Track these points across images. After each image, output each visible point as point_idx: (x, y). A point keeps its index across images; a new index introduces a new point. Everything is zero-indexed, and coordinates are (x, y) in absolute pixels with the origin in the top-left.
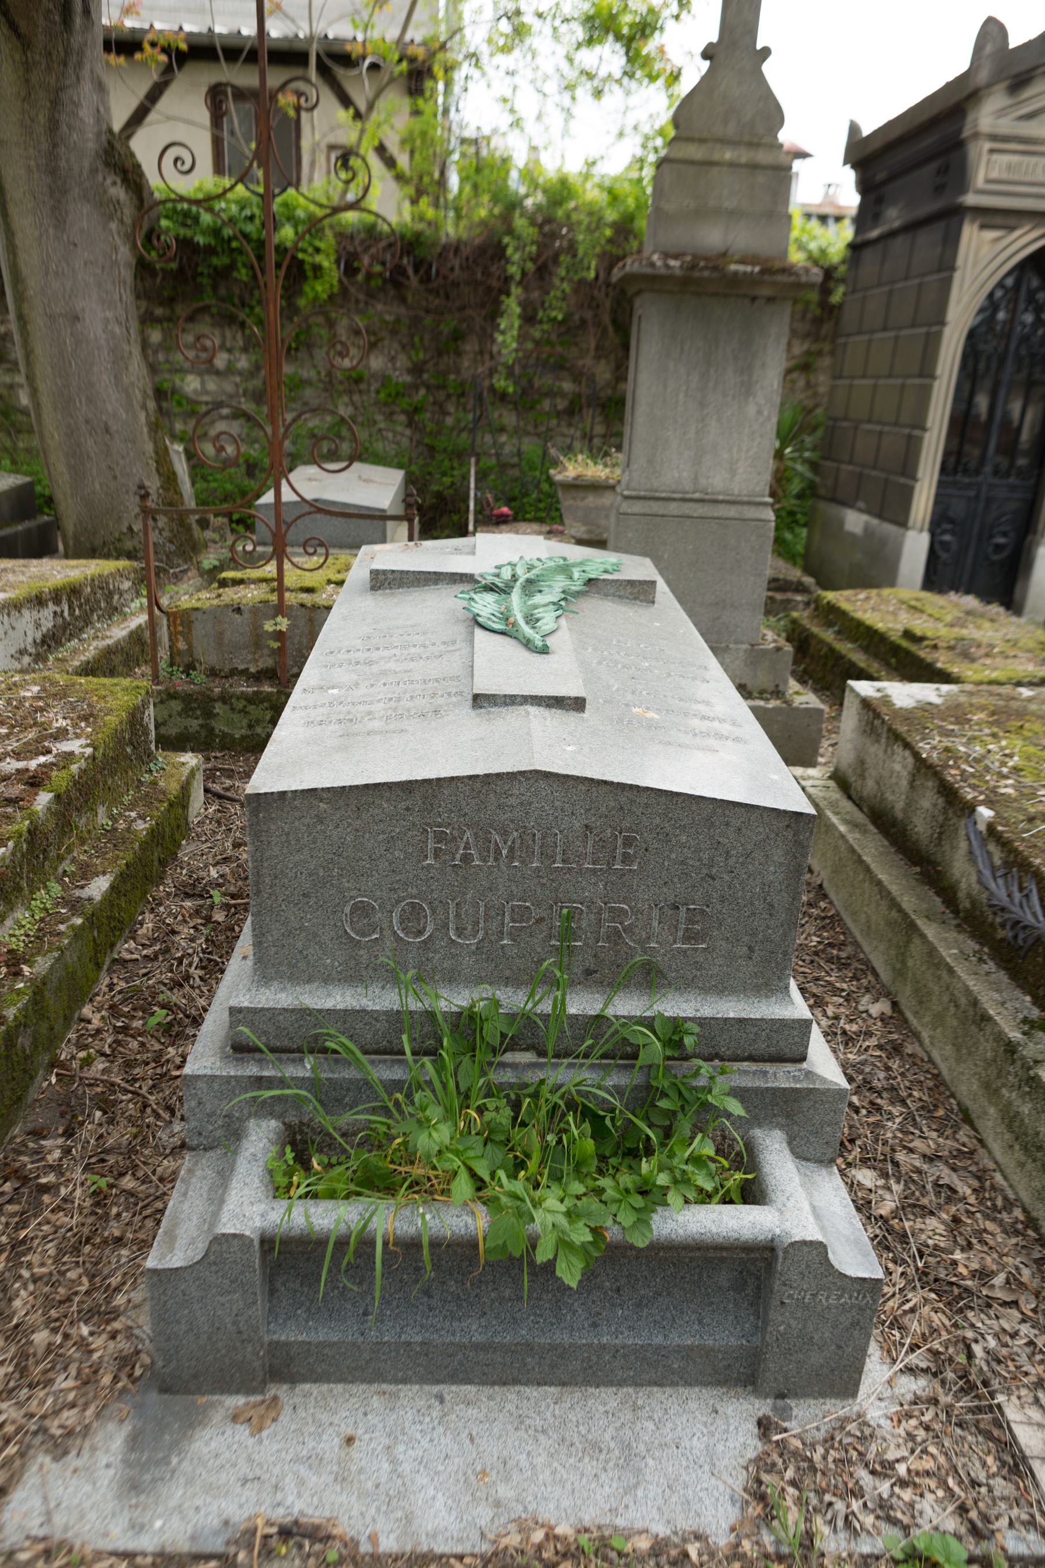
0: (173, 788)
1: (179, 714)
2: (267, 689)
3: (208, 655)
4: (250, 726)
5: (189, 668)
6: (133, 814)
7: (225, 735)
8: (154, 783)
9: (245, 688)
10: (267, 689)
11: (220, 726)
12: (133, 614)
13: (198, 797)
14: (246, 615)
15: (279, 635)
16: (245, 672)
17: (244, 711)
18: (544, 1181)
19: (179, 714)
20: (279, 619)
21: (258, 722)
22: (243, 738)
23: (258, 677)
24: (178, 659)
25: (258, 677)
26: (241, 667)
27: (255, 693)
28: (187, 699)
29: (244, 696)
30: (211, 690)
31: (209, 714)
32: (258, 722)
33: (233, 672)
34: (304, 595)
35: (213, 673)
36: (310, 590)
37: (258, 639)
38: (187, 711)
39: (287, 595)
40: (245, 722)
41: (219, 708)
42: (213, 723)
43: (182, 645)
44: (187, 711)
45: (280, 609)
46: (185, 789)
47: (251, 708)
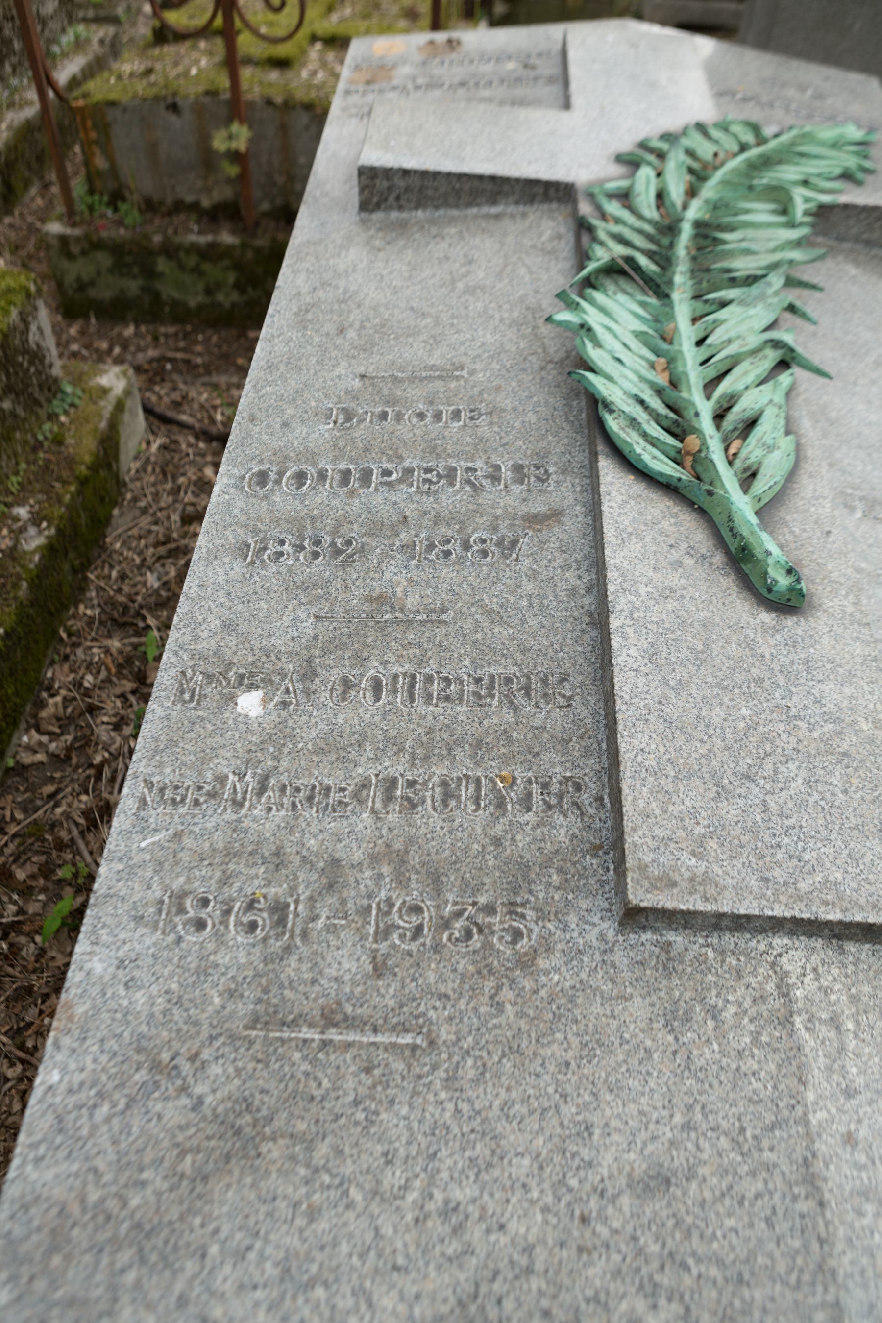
0: (83, 446)
1: (111, 271)
2: (227, 238)
3: (141, 181)
4: (209, 292)
5: (116, 198)
6: (22, 512)
7: (175, 304)
8: (58, 441)
9: (196, 236)
10: (227, 238)
11: (168, 291)
12: (65, 55)
13: (136, 424)
14: (188, 116)
15: (235, 156)
16: (195, 207)
17: (196, 271)
18: (586, 1154)
19: (111, 271)
20: (235, 127)
21: (218, 286)
22: (201, 307)
23: (217, 215)
24: (98, 184)
25: (217, 215)
26: (189, 198)
27: (212, 245)
28: (117, 250)
29: (194, 248)
30: (147, 237)
31: (150, 274)
32: (218, 286)
33: (179, 207)
34: (274, 75)
35: (150, 206)
36: (282, 64)
37: (208, 160)
38: (120, 268)
39: (246, 73)
40: (200, 286)
41: (162, 265)
42: (159, 285)
43: (100, 162)
44: (120, 268)
45: (235, 108)
46: (109, 443)
47: (206, 266)
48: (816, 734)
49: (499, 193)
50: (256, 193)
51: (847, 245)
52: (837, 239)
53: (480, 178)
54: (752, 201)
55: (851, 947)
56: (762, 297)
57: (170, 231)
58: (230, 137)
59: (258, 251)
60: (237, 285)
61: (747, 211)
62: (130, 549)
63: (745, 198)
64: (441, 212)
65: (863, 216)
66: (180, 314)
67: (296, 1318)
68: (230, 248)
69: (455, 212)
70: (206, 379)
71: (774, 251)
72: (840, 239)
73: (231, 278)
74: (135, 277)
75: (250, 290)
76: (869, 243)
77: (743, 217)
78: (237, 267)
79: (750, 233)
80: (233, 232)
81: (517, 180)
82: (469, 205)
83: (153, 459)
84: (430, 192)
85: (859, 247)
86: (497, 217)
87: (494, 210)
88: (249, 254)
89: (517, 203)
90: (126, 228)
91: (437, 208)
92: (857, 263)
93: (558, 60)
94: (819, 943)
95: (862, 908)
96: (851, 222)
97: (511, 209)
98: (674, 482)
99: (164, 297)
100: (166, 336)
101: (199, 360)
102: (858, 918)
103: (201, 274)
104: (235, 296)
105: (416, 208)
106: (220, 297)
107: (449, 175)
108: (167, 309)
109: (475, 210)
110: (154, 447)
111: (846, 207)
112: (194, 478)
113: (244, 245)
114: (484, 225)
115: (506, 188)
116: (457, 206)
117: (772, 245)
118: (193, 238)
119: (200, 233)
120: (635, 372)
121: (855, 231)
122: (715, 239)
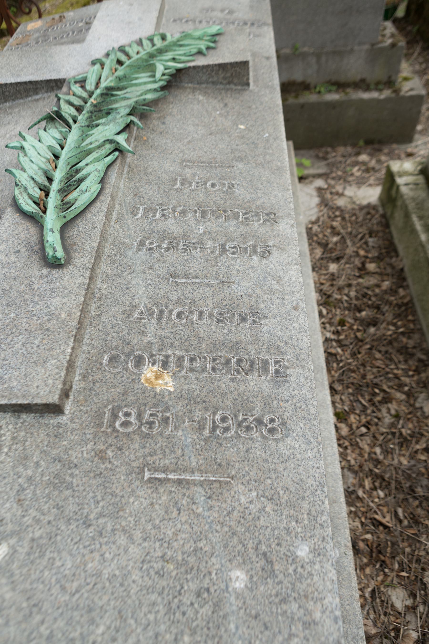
48: (39, 321)
49: (37, 89)
51: (204, 86)
52: (198, 84)
53: (25, 83)
54: (140, 73)
55: (24, 416)
56: (114, 119)
61: (137, 78)
63: (137, 72)
64: (16, 102)
65: (205, 70)
67: (92, 638)
69: (22, 101)
71: (141, 95)
72: (200, 83)
76: (213, 83)
77: (134, 82)
79: (133, 88)
81: (42, 81)
82: (27, 96)
84: (7, 94)
85: (210, 85)
86: (37, 100)
87: (38, 97)
89: (47, 92)
91: (14, 100)
92: (205, 94)
94: (8, 415)
95: (18, 397)
96: (201, 74)
97: (45, 95)
98: (34, 215)
102: (14, 402)
105: (5, 102)
107: (11, 84)
109: (30, 99)
111: (194, 67)
114: (30, 105)
115: (39, 86)
116: (22, 98)
117: (138, 93)
120: (37, 165)
121: (204, 78)
122: (112, 95)
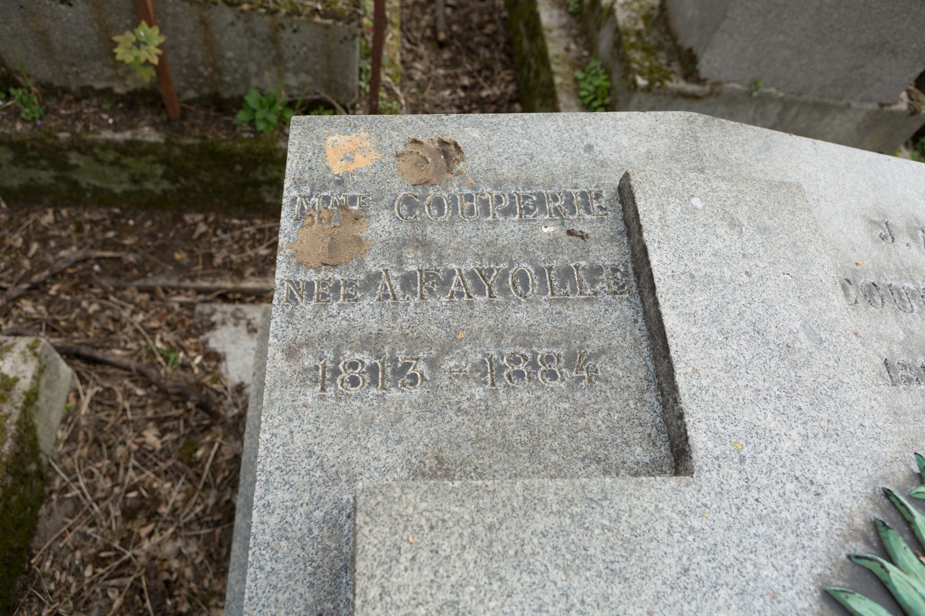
2: (149, 135)
10: (149, 135)
11: (86, 180)
16: (107, 93)
20: (143, 30)
21: (145, 176)
22: (127, 194)
26: (98, 85)
27: (130, 143)
29: (109, 145)
33: (86, 93)
40: (124, 176)
41: (74, 158)
50: (177, 83)
57: (79, 127)
58: (138, 44)
59: (187, 148)
60: (165, 176)
62: (63, 569)
66: (102, 198)
68: (152, 148)
70: (141, 282)
73: (159, 170)
74: (44, 169)
75: (182, 180)
78: (164, 161)
80: (154, 125)
83: (84, 422)
88: (177, 151)
90: (24, 121)
93: (613, 222)
99: (84, 185)
100: (94, 223)
101: (131, 258)
103: (124, 167)
104: (165, 185)
106: (149, 185)
108: (89, 195)
110: (86, 401)
112: (135, 447)
113: (168, 143)
118: (107, 135)
119: (116, 128)
